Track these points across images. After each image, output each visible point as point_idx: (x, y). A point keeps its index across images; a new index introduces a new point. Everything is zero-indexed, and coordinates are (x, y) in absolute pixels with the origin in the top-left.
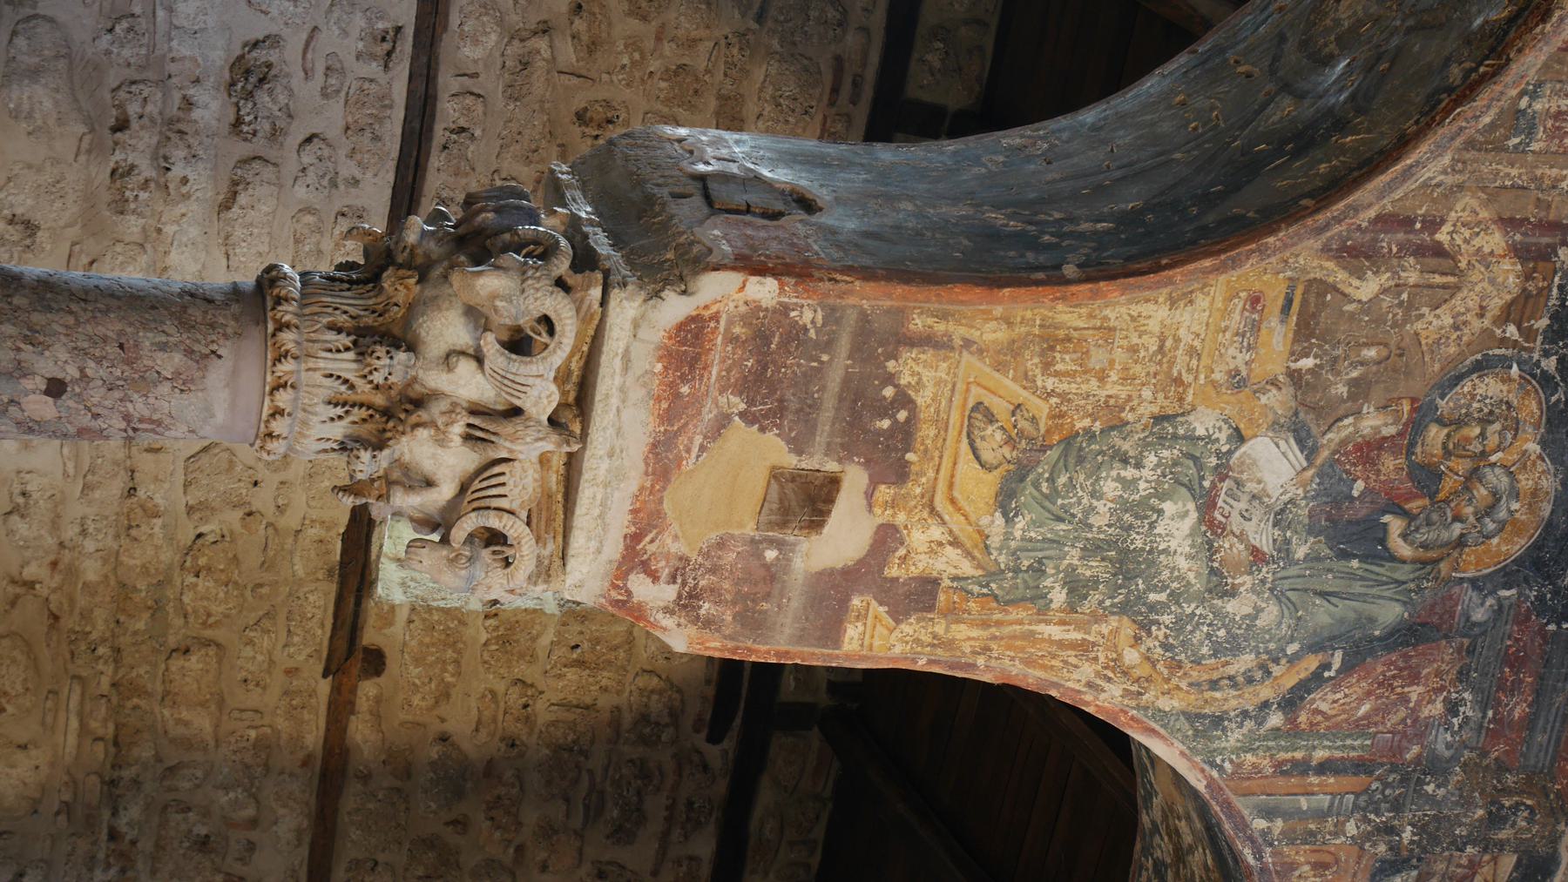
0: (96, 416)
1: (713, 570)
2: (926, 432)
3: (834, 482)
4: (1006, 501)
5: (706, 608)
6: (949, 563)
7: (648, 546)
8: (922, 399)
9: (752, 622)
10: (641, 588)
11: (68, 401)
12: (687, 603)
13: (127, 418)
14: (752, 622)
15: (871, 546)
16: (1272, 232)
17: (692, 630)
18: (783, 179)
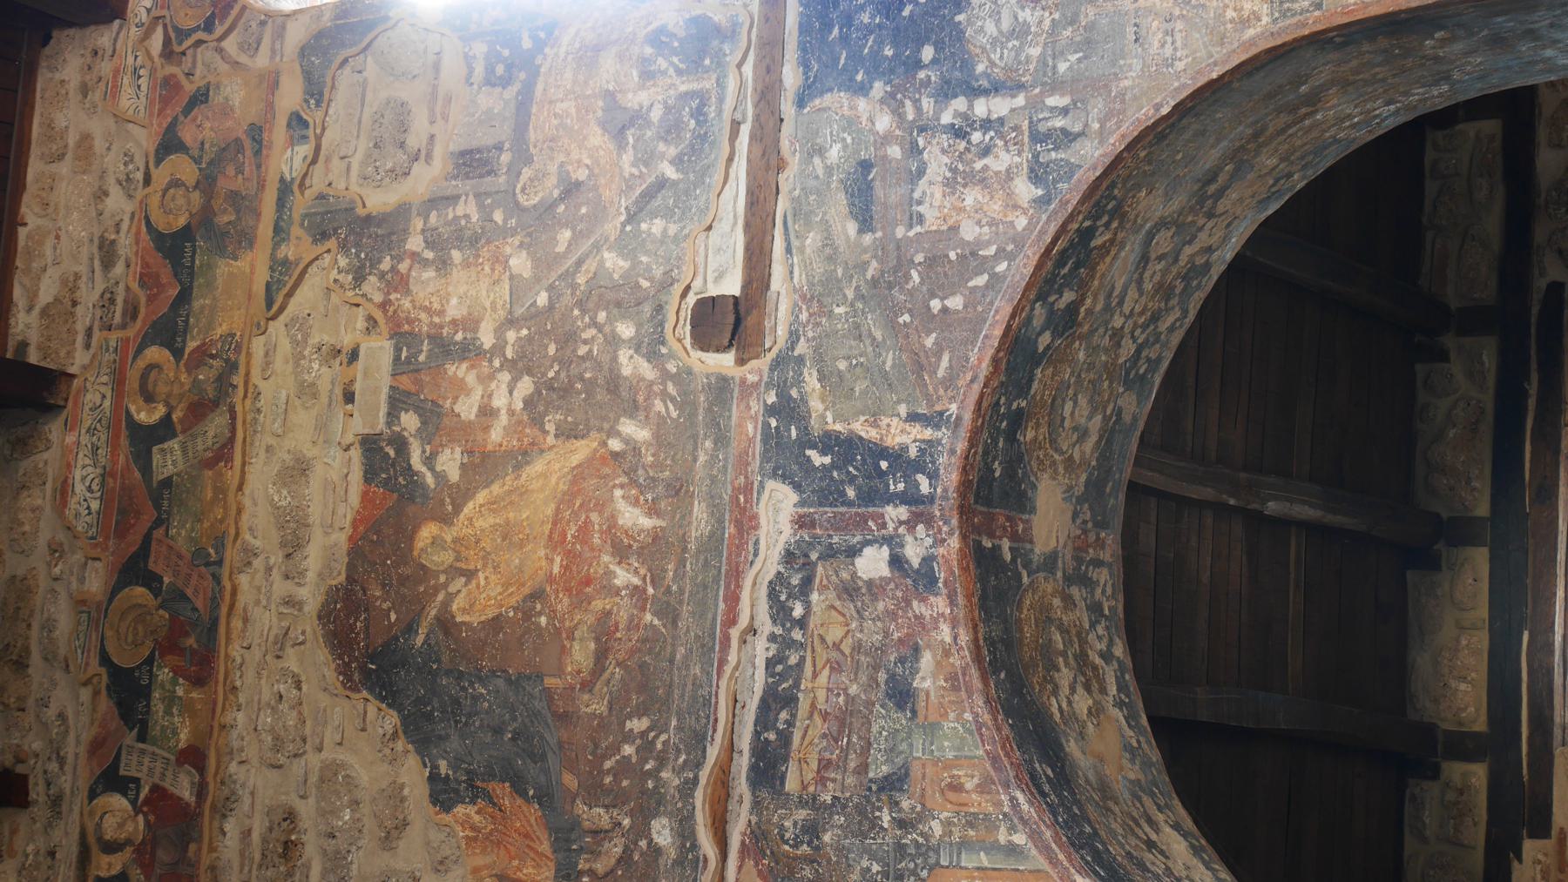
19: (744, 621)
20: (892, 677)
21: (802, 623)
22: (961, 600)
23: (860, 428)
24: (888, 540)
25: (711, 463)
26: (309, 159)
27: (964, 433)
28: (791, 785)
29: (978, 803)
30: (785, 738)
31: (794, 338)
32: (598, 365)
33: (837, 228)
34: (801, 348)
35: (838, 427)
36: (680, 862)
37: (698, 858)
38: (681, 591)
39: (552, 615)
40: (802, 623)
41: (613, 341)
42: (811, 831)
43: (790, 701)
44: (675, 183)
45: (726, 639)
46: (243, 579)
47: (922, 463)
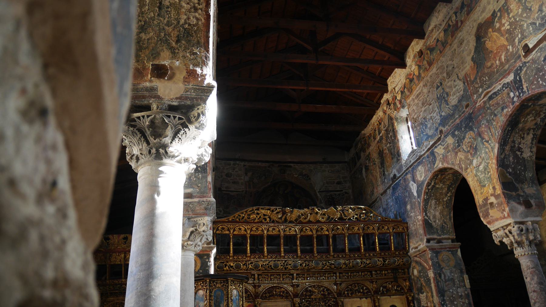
0: (528, 273)
1: (500, 210)
2: (484, 197)
3: (490, 203)
5: (503, 208)
6: (491, 187)
7: (503, 217)
8: (482, 200)
9: (502, 204)
11: (527, 276)
12: (504, 210)
13: (527, 270)
15: (209, 271)
17: (505, 208)
18: (496, 151)
19: (501, 82)
20: (503, 106)
21: (503, 90)
22: (513, 109)
23: (523, 80)
24: (515, 95)
25: (512, 63)
26: (445, 158)
27: (529, 95)
28: (490, 102)
29: (498, 126)
30: (493, 98)
31: (528, 62)
32: (515, 36)
33: (542, 57)
34: (527, 64)
35: (522, 78)
36: (479, 94)
37: (193, 88)
38: (500, 71)
39: (491, 56)
40: (503, 90)
41: (518, 35)
44: (536, 26)
45: (498, 82)
46: (478, 8)
47: (524, 92)
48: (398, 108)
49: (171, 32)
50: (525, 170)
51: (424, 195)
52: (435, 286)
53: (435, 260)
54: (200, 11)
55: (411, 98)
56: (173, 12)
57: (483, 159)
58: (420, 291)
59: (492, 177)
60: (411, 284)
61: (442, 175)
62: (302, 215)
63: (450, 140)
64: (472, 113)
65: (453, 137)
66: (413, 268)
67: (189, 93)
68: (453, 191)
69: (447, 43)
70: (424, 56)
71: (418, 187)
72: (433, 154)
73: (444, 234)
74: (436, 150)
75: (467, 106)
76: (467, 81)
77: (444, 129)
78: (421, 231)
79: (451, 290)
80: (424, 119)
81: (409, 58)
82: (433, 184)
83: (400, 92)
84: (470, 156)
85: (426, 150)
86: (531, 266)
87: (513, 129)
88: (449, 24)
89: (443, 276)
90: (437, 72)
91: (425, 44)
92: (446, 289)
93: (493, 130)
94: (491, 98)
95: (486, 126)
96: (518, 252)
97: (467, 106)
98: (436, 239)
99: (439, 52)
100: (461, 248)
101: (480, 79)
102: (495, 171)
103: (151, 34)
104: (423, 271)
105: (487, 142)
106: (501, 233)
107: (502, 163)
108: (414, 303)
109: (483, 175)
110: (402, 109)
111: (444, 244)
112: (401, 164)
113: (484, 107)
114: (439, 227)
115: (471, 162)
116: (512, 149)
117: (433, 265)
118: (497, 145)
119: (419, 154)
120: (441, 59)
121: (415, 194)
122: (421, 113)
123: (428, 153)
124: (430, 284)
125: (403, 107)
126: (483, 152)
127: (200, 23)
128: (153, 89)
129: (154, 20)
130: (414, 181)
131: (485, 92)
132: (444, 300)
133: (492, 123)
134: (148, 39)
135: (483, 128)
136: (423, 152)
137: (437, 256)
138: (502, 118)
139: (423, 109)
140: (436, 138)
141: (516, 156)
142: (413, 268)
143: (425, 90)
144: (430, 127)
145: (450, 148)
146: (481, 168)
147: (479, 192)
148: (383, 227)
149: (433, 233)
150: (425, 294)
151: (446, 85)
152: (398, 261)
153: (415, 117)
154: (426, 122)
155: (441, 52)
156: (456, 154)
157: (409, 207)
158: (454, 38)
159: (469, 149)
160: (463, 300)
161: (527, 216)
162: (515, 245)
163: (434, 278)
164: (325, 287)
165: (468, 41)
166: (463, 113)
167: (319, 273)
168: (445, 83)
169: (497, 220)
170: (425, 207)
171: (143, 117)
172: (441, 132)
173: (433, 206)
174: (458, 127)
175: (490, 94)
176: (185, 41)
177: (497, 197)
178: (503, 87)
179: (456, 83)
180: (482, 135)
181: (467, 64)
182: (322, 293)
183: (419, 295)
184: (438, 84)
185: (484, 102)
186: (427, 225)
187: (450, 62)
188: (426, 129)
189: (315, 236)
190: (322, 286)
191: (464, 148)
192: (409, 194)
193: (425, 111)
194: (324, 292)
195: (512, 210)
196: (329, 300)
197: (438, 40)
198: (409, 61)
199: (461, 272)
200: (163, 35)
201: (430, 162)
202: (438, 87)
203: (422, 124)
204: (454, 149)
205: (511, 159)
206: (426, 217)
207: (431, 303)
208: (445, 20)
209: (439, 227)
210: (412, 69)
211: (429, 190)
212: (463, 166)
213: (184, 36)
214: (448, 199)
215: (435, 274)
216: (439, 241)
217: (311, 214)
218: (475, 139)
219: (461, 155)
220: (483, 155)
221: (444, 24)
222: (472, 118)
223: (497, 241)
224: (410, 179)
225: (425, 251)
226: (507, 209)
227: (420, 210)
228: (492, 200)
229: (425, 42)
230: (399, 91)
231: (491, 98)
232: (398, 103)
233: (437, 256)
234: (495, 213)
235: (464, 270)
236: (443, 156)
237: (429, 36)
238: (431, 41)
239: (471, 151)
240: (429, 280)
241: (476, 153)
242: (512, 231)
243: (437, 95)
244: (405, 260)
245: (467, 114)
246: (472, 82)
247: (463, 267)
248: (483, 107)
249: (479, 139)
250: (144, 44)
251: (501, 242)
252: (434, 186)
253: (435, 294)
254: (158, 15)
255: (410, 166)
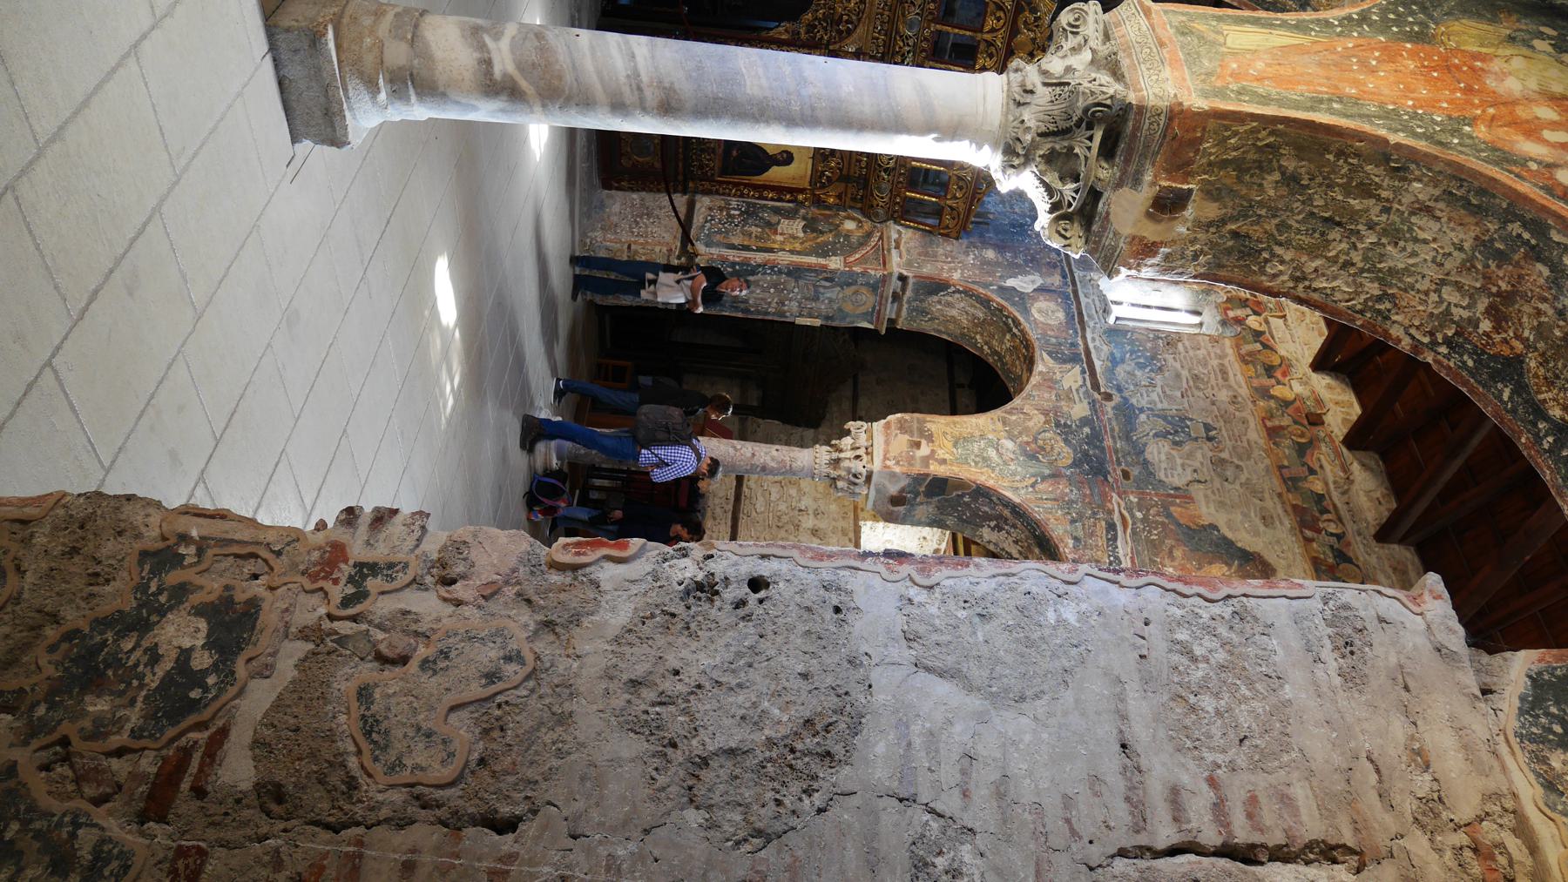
4: (955, 446)
6: (947, 456)
9: (911, 465)
10: (888, 463)
12: (898, 463)
14: (911, 465)
16: (679, 305)
18: (1009, 494)
28: (1103, 523)
30: (1108, 532)
42: (1094, 513)
43: (1108, 540)
48: (1228, 309)
49: (1262, 227)
50: (960, 519)
51: (998, 304)
52: (810, 265)
53: (860, 280)
54: (1291, 284)
55: (1230, 351)
56: (1307, 240)
57: (1005, 463)
58: (811, 226)
59: (965, 467)
60: (829, 207)
61: (1025, 357)
62: (1037, 19)
63: (1080, 410)
64: (1106, 479)
65: (1081, 419)
66: (860, 221)
67: (1111, 236)
68: (991, 360)
69: (1289, 490)
70: (1302, 425)
71: (1022, 295)
72: (1075, 359)
73: (910, 311)
74: (1078, 369)
75: (1126, 475)
76: (1176, 497)
77: (1109, 406)
78: (927, 270)
79: (796, 290)
80: (1160, 368)
81: (1329, 387)
82: (1015, 330)
83: (1264, 328)
84: (1025, 439)
85: (1091, 346)
86: (794, 465)
87: (1035, 537)
88: (1328, 512)
89: (828, 284)
90: (1244, 439)
91: (1327, 439)
92: (801, 282)
93: (1049, 505)
94: (1111, 527)
95: (1065, 495)
96: (822, 453)
97: (1126, 475)
98: (904, 293)
99: (1286, 463)
100: (876, 331)
101: (1163, 524)
102: (973, 478)
103: (1272, 193)
104: (846, 246)
105: (1033, 486)
106: (863, 440)
107: (982, 492)
108: (789, 201)
109: (976, 450)
110: (1219, 318)
111: (889, 305)
112: (1092, 270)
113: (1102, 506)
114: (925, 305)
115: (1011, 437)
116: (1000, 517)
117: (852, 274)
118: (1017, 500)
119: (1092, 324)
120: (1267, 461)
121: (1010, 283)
122: (1178, 365)
123: (1081, 347)
124: (818, 255)
125: (1224, 323)
126: (1019, 469)
127: (1264, 278)
128: (1136, 182)
129: (1303, 203)
130: (1041, 290)
131: (1130, 522)
132: (780, 272)
133: (1062, 509)
134: (1261, 185)
135: (1063, 487)
136: (1089, 336)
137: (867, 284)
138: (1061, 532)
139: (1185, 373)
140: (1102, 381)
141: (988, 517)
142: (860, 221)
143: (1223, 396)
144: (1134, 375)
145: (1063, 403)
146: (992, 453)
147: (948, 430)
148: (961, 188)
149: (916, 291)
150: (801, 235)
151: (1201, 448)
152: (881, 199)
153: (1180, 345)
154: (1152, 370)
155: (1281, 467)
156: (1045, 413)
157: (990, 254)
158: (1289, 509)
159: (1040, 442)
160: (774, 305)
161: (878, 491)
162: (835, 455)
163: (825, 266)
164: (856, 27)
165: (1257, 534)
166: (1118, 459)
167: (892, 21)
168: (1205, 448)
169: (887, 443)
170: (973, 295)
171: (1089, 148)
172: (1108, 397)
173: (972, 310)
174: (1095, 438)
175: (1119, 528)
176: (1232, 247)
177: (926, 460)
178: (1117, 558)
179: (1189, 471)
180: (1050, 481)
181: (1212, 510)
182: (845, 18)
183: (804, 218)
184: (1214, 432)
185: (1110, 512)
186: (936, 286)
187: (1243, 478)
188: (1137, 364)
189: (979, 36)
190: (859, 20)
191: (1047, 434)
192: (1018, 266)
193: (1178, 376)
194: (847, 22)
195: (893, 476)
196: (825, 29)
197: (1312, 472)
198: (1322, 384)
199: (827, 318)
200: (1259, 212)
201: (1060, 344)
202: (1208, 427)
203: (1153, 358)
204: (1056, 410)
205: (986, 509)
206: (953, 289)
207: (782, 243)
208: (1345, 507)
209: (925, 305)
210: (1295, 384)
211: (1007, 317)
212: (1014, 418)
213: (1245, 247)
214: (976, 342)
215: (833, 272)
216: (896, 297)
217: (1034, 40)
218: (1051, 463)
219: (1037, 420)
220: (1013, 467)
221: (1339, 505)
222: (1095, 474)
223: (851, 425)
224: (1049, 281)
225: (884, 264)
226: (897, 470)
227: (973, 282)
228: (925, 450)
229: (1332, 441)
230: (1269, 328)
231: (1111, 527)
232: (1239, 313)
233: (867, 284)
234: (901, 442)
235: (829, 323)
236: (1057, 382)
237: (1339, 455)
238: (1324, 457)
239: (1033, 446)
240: (825, 255)
241: (1025, 453)
242: (858, 461)
243: (1191, 420)
244: (881, 211)
245: (1110, 469)
246: (1166, 508)
247: (835, 324)
248: (1102, 505)
249: (1047, 472)
250: (1252, 176)
251: (848, 433)
252: (1010, 330)
253: (796, 258)
254: (1312, 214)
255: (1075, 292)
